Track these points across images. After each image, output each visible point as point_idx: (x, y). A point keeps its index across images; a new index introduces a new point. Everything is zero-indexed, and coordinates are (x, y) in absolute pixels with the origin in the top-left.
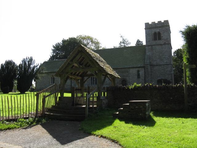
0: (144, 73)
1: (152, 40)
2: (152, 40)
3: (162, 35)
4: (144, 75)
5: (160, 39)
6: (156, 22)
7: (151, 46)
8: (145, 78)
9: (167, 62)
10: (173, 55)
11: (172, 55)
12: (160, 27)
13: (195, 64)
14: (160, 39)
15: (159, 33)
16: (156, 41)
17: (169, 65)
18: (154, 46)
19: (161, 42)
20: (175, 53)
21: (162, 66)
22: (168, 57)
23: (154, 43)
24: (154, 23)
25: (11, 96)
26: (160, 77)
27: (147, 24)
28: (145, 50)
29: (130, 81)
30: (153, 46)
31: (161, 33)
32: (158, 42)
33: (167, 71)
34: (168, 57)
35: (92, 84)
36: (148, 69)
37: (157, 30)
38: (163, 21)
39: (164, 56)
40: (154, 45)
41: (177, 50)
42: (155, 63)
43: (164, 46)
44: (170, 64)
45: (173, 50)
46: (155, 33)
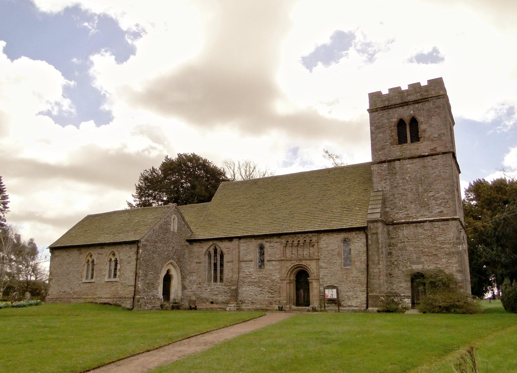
0: (365, 249)
1: (392, 144)
2: (392, 144)
3: (422, 127)
4: (365, 255)
5: (416, 138)
6: (405, 88)
7: (389, 161)
8: (368, 265)
9: (442, 212)
10: (463, 196)
11: (459, 196)
12: (416, 102)
13: (370, 167)
14: (416, 138)
15: (414, 122)
16: (405, 146)
17: (450, 222)
18: (397, 163)
19: (423, 147)
20: (468, 191)
21: (427, 226)
22: (447, 197)
23: (397, 151)
24: (396, 91)
25: (262, 248)
26: (419, 263)
27: (374, 97)
28: (371, 173)
29: (321, 275)
30: (394, 160)
31: (420, 119)
32: (411, 148)
33: (443, 243)
34: (447, 197)
35: (209, 281)
36: (377, 234)
37: (406, 113)
38: (424, 83)
39: (431, 194)
40: (399, 160)
41: (474, 182)
42: (400, 216)
43: (429, 159)
44: (455, 219)
45: (464, 184)
46: (401, 123)
